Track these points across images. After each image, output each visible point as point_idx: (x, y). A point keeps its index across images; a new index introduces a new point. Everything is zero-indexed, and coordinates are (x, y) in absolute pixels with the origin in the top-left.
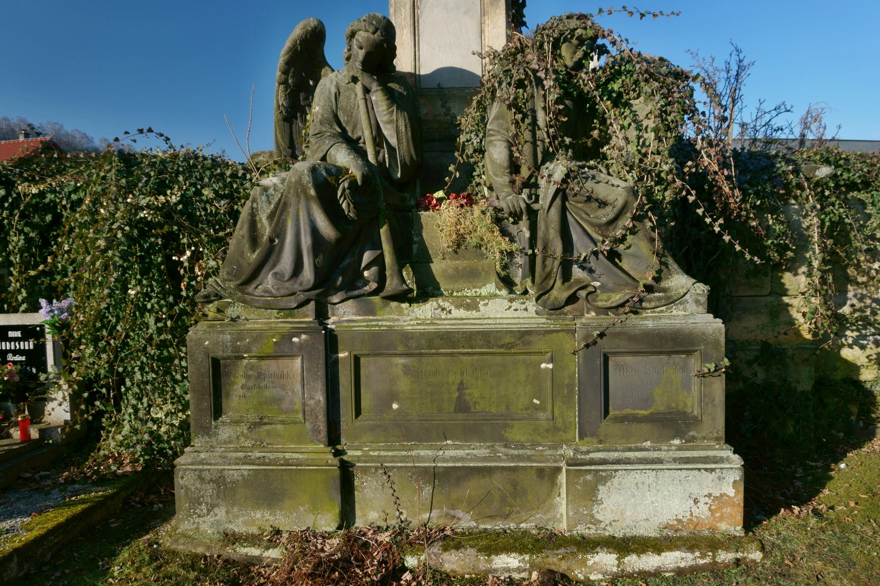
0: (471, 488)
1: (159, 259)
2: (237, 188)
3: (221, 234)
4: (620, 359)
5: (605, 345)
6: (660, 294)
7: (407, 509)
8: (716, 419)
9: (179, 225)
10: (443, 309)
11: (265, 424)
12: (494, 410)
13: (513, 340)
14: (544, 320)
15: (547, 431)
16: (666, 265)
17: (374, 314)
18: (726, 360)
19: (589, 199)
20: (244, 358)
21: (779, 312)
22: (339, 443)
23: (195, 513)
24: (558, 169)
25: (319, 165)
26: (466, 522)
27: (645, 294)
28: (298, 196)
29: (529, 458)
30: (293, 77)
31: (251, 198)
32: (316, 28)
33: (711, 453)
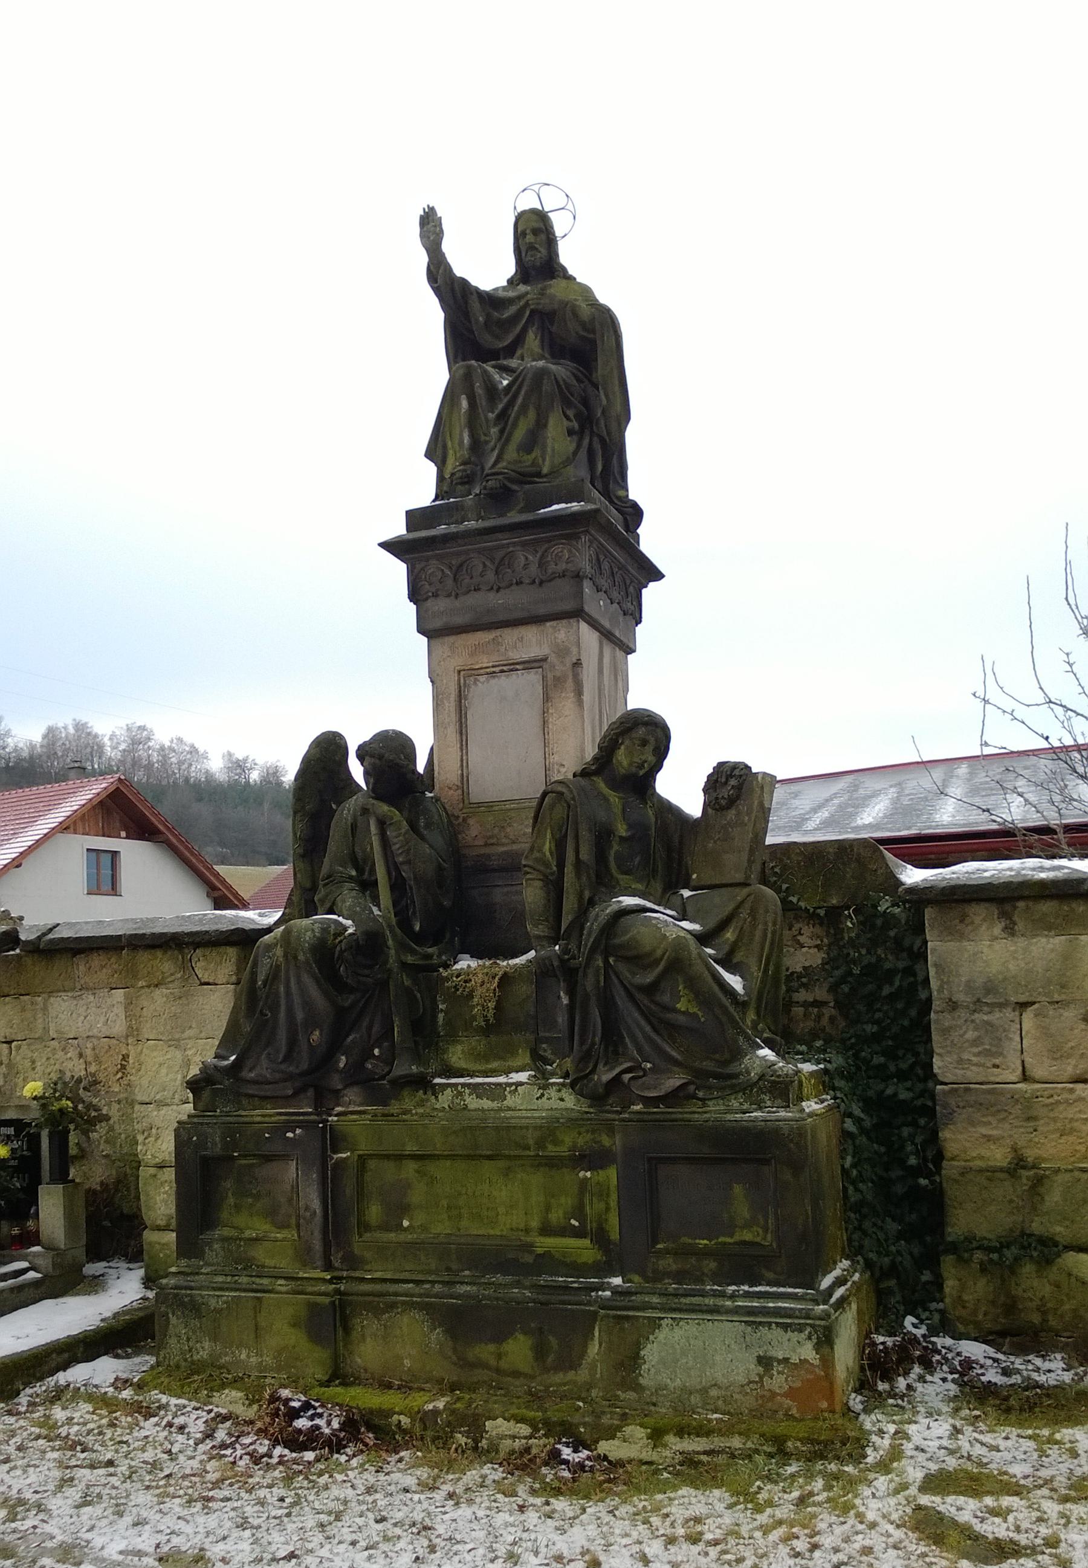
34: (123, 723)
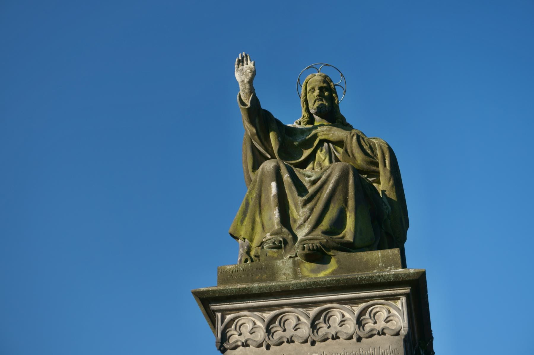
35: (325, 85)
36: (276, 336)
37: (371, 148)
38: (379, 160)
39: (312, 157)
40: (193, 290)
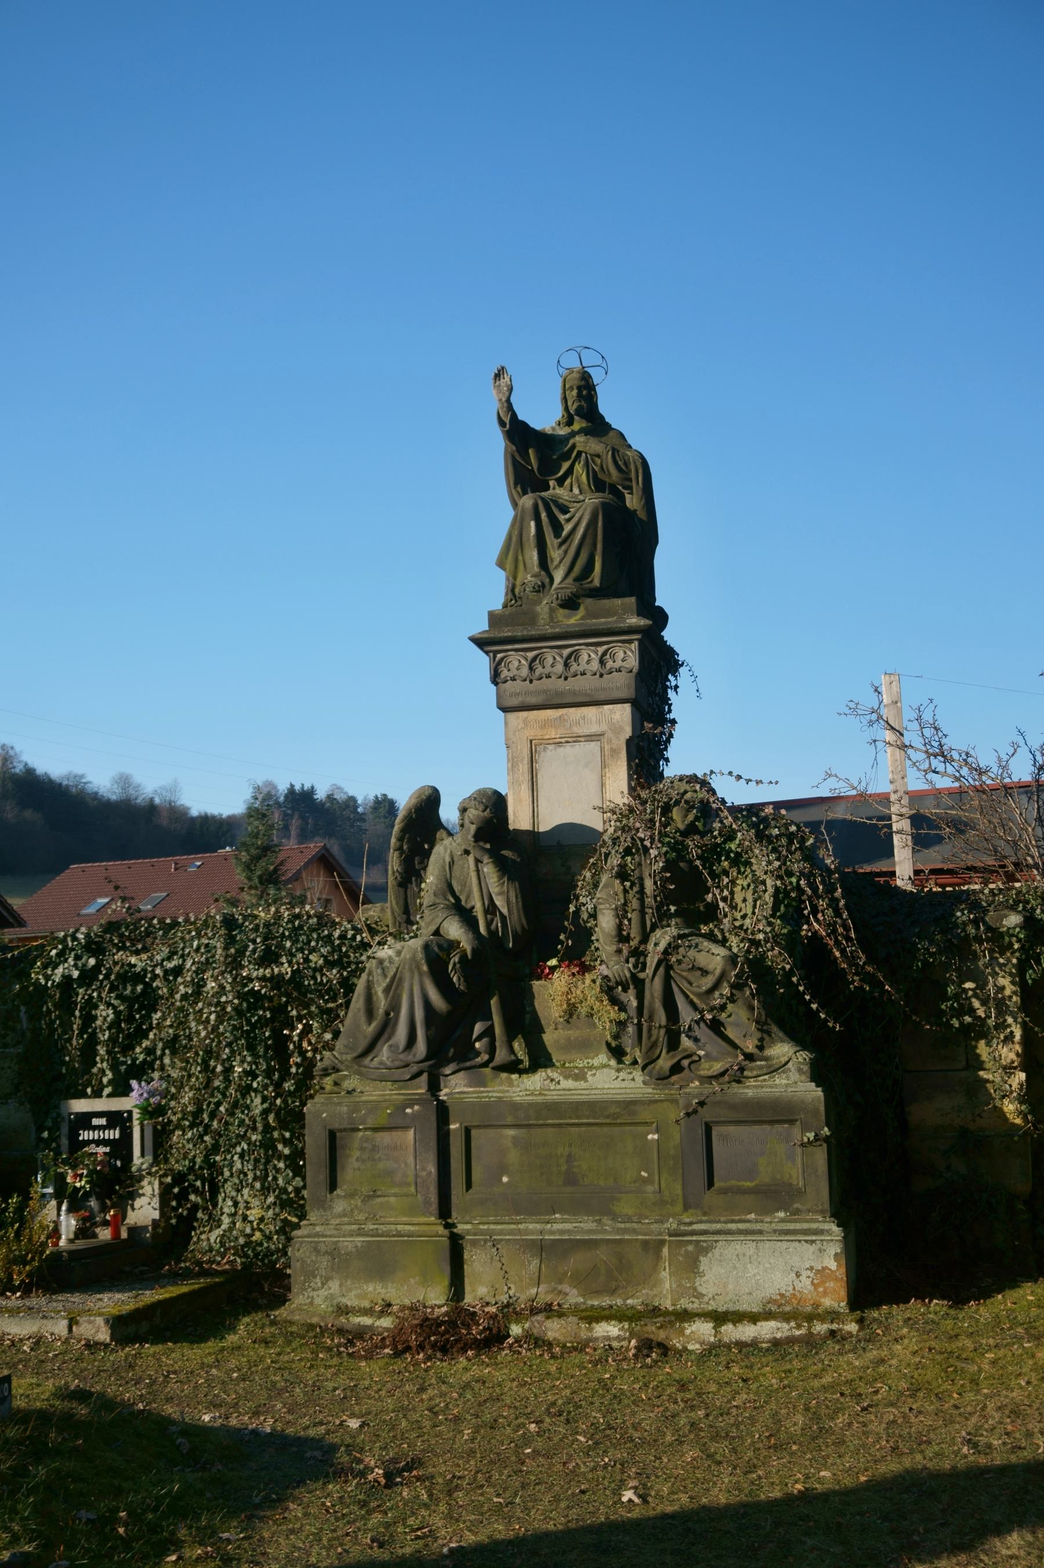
0: (577, 1261)
1: (267, 1034)
2: (347, 951)
3: (331, 1005)
4: (723, 1129)
5: (706, 1114)
6: (762, 1063)
7: (515, 1284)
8: (821, 1190)
9: (288, 995)
10: (552, 1080)
11: (379, 1196)
12: (602, 1183)
13: (618, 1110)
14: (650, 1091)
15: (654, 1204)
16: (769, 1033)
17: (485, 1086)
18: (826, 1129)
19: (694, 968)
20: (359, 1130)
21: (976, 1090)
22: (450, 1217)
23: (309, 1287)
24: (662, 938)
25: (432, 941)
26: (574, 1297)
27: (747, 1062)
28: (412, 972)
29: (635, 1231)
30: (408, 842)
31: (367, 971)
32: (430, 796)
33: (814, 1226)
34: (265, 779)
35: (583, 383)
36: (537, 673)
37: (625, 464)
38: (633, 475)
39: (570, 471)
40: (471, 634)
